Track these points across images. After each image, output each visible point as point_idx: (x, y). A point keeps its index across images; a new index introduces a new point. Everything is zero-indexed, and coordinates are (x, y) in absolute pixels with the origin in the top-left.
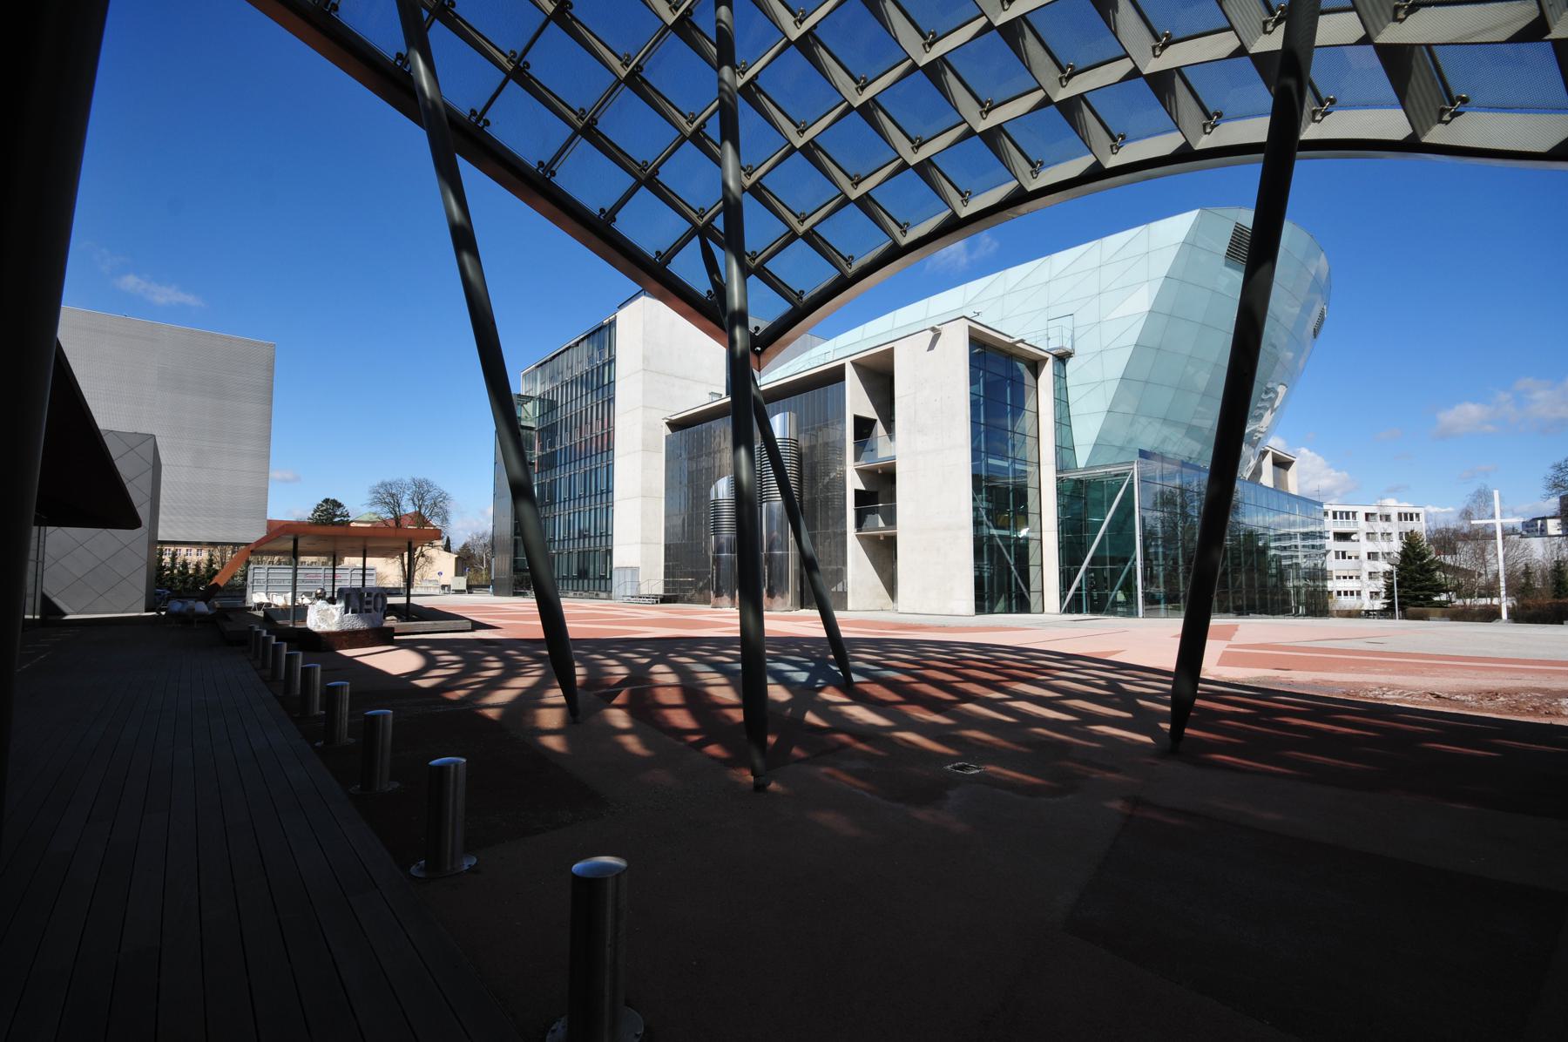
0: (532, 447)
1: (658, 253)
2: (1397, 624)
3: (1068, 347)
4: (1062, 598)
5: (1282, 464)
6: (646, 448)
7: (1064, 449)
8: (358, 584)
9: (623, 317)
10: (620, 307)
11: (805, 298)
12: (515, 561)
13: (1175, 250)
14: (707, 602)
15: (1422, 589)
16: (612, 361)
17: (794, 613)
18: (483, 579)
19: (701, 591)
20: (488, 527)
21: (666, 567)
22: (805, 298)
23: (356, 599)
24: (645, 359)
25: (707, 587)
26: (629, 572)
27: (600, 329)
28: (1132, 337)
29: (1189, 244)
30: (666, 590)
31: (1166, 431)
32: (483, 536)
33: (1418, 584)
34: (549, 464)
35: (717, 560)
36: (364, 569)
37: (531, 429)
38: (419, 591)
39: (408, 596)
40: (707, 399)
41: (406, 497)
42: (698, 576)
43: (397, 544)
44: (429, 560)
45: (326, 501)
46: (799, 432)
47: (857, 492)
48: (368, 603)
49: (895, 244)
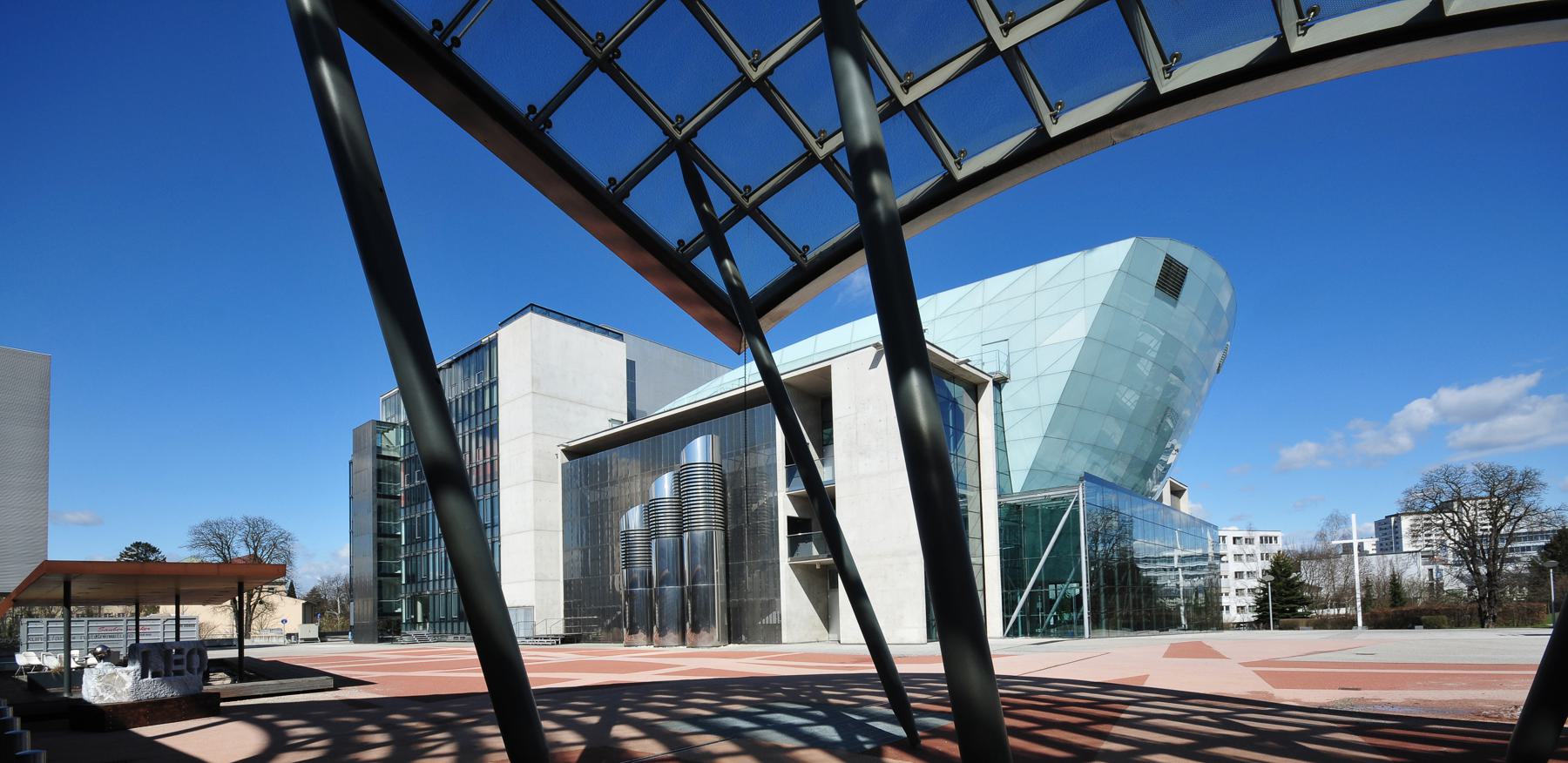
0: (396, 479)
1: (612, 181)
2: (1273, 635)
3: (1004, 371)
4: (1006, 621)
5: (1177, 492)
6: (538, 478)
7: (1003, 473)
8: (171, 637)
9: (506, 336)
10: (502, 324)
11: (810, 256)
12: (380, 605)
13: (1110, 279)
14: (620, 641)
15: (1288, 602)
16: (494, 384)
17: (723, 649)
18: (338, 627)
19: (609, 628)
20: (345, 570)
21: (566, 605)
22: (810, 256)
23: (150, 658)
24: (534, 380)
25: (618, 623)
26: (521, 611)
27: (477, 349)
28: (1069, 363)
29: (1127, 272)
30: (567, 630)
31: (1096, 457)
32: (336, 580)
33: (1284, 599)
34: (433, 486)
35: (630, 596)
36: (178, 618)
37: (395, 459)
38: (257, 641)
39: (241, 648)
40: (608, 425)
41: (237, 538)
42: (604, 614)
43: (220, 586)
44: (270, 607)
45: (137, 545)
46: (723, 457)
47: (790, 519)
48: (178, 662)
49: (949, 177)
